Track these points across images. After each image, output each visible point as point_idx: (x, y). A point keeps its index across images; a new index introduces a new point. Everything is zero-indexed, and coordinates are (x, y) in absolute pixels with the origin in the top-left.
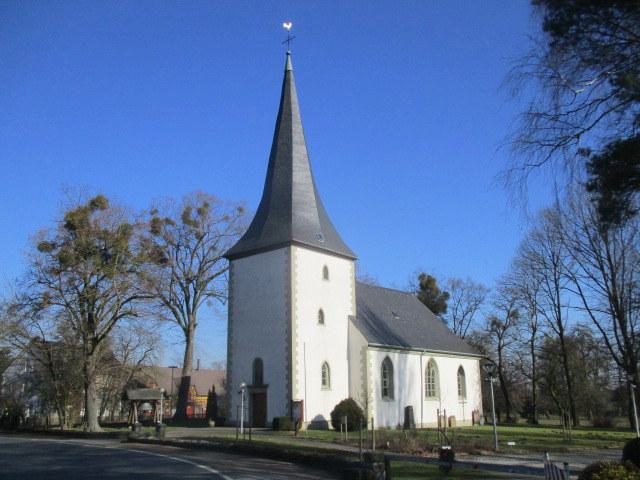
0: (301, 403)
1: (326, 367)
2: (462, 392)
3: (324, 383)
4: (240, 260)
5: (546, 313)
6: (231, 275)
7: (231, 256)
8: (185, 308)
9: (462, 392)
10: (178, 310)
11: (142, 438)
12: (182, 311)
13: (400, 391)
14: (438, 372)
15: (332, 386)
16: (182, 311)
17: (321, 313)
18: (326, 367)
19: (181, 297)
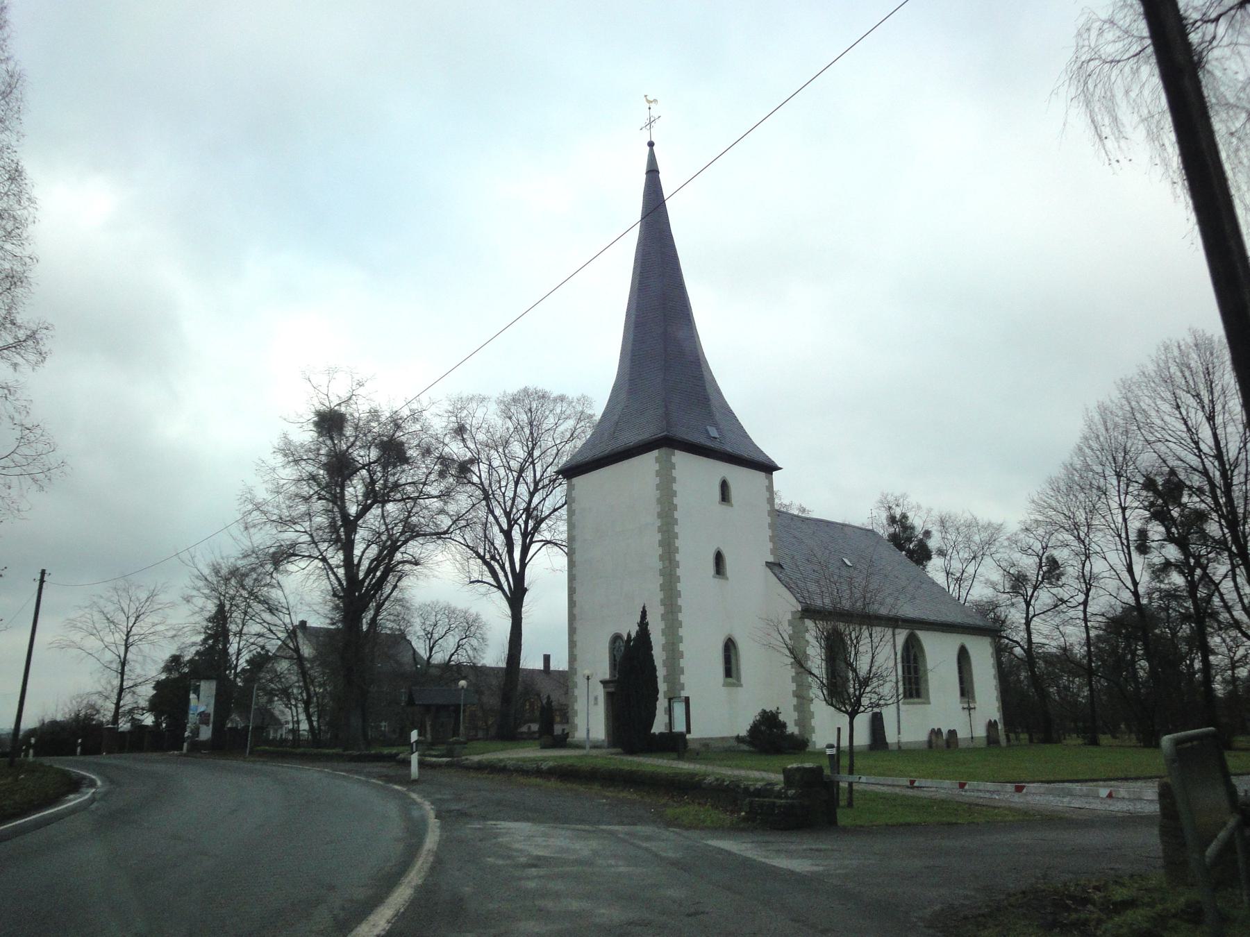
0: (657, 477)
1: (730, 647)
2: (966, 690)
3: (728, 672)
4: (684, 707)
5: (1108, 555)
6: (571, 513)
7: (570, 472)
8: (507, 565)
9: (966, 690)
10: (497, 567)
11: (1242, 593)
12: (503, 568)
13: (288, 767)
14: (924, 656)
15: (743, 680)
16: (503, 568)
17: (719, 558)
18: (730, 647)
19: (503, 550)
